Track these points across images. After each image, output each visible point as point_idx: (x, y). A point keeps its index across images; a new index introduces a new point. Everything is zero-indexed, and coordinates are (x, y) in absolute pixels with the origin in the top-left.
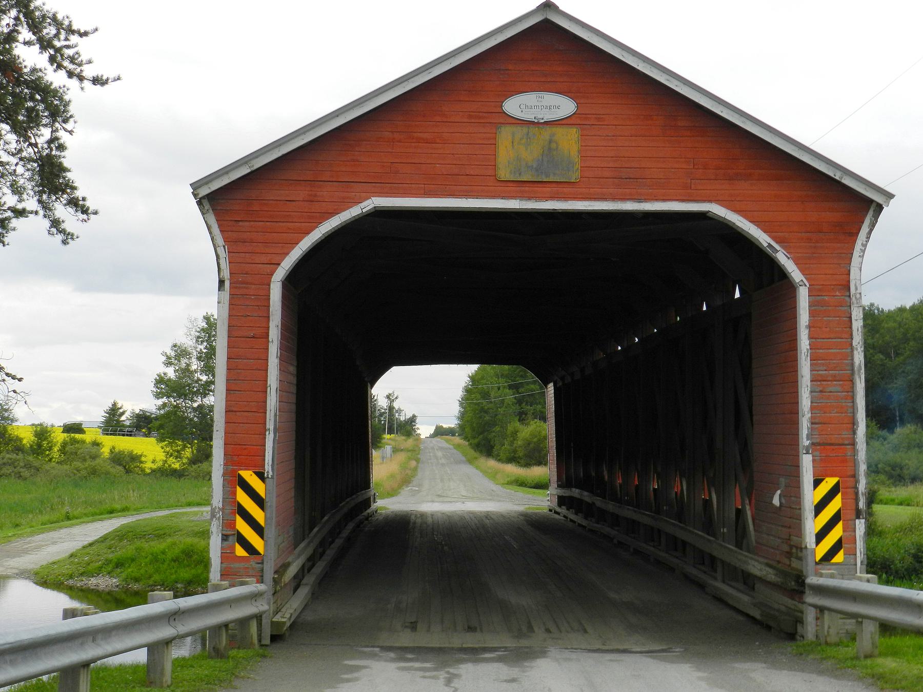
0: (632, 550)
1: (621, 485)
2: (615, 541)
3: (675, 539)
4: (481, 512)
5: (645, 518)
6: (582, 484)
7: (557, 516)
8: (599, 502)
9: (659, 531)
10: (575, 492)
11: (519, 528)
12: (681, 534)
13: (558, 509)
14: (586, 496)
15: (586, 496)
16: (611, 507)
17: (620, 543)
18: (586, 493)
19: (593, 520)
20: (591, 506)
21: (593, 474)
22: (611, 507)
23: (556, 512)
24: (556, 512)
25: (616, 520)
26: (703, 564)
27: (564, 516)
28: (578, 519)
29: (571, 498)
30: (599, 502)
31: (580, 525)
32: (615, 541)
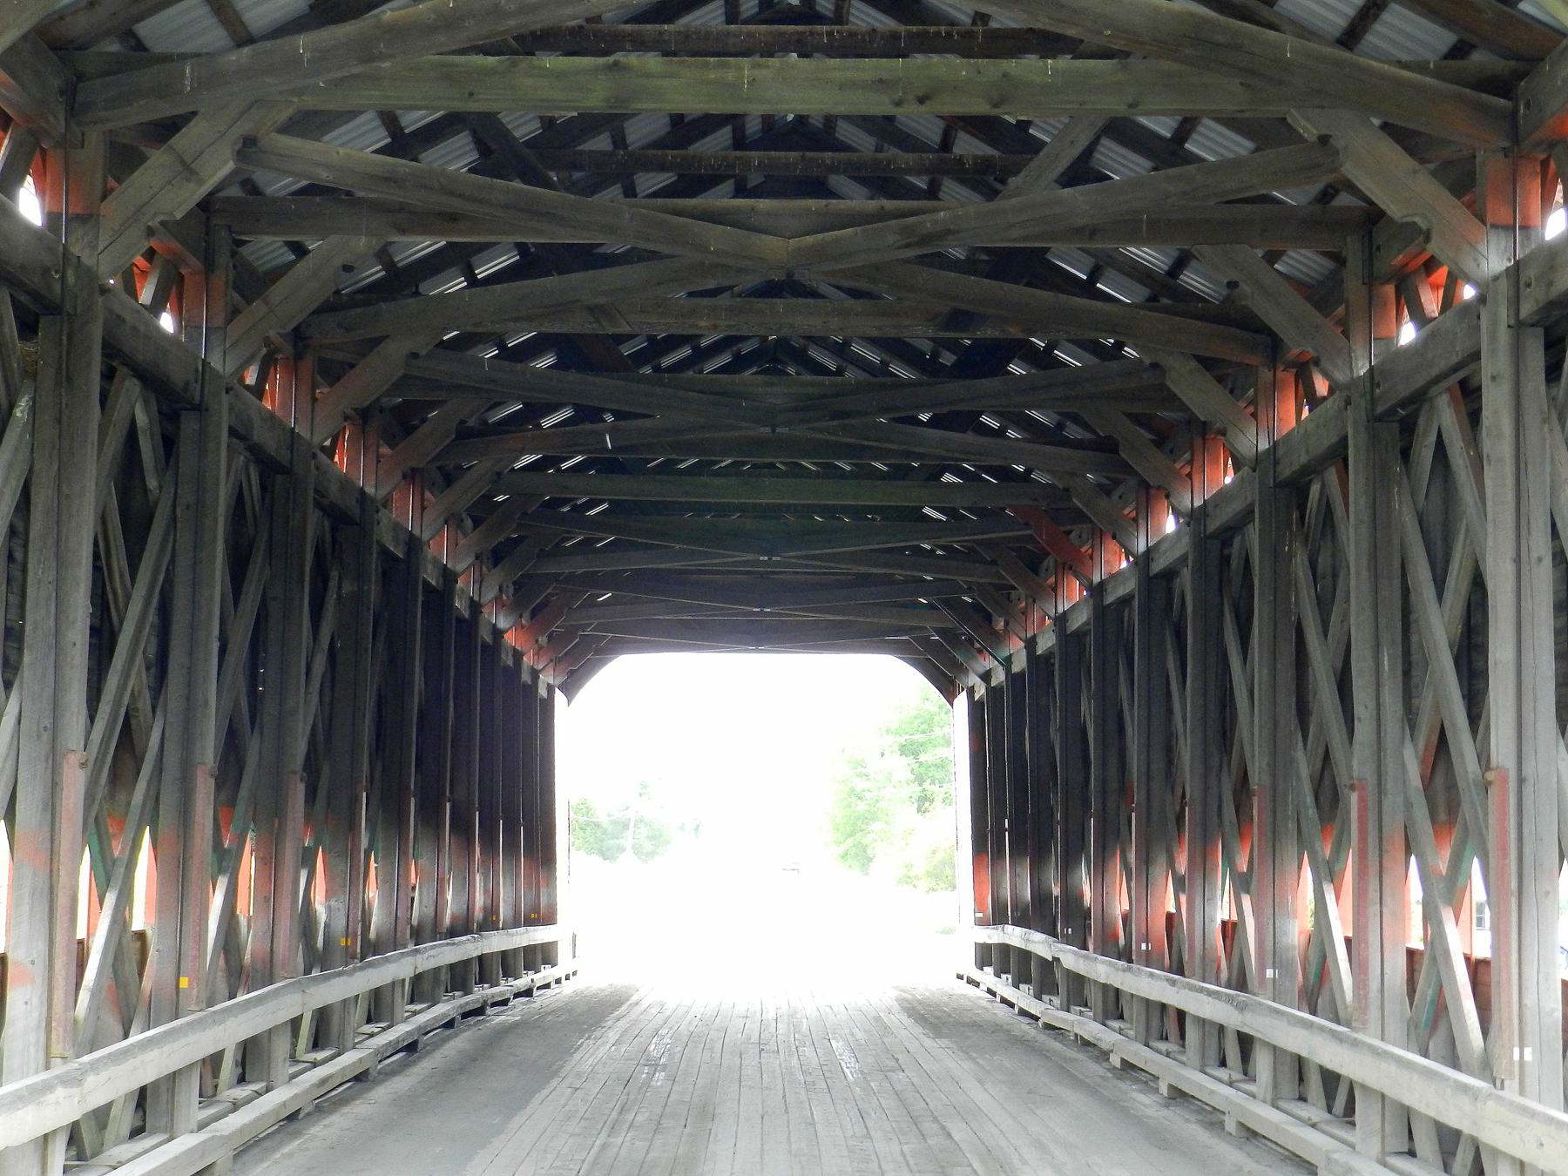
0: (1164, 1090)
1: (1126, 919)
2: (1115, 1060)
3: (1300, 1063)
4: (610, 660)
5: (1202, 1002)
6: (1037, 914)
7: (971, 990)
8: (1070, 958)
9: (1181, 1015)
10: (1014, 936)
11: (878, 1019)
12: (1326, 1053)
13: (976, 974)
14: (1039, 943)
15: (1039, 943)
16: (1101, 969)
17: (1127, 1066)
18: (1038, 937)
19: (1057, 1001)
20: (1049, 966)
21: (1056, 891)
22: (1101, 969)
23: (970, 981)
24: (970, 981)
25: (1114, 1005)
26: (1223, 1064)
27: (990, 991)
28: (1023, 997)
29: (1005, 949)
30: (1070, 958)
31: (1023, 1013)
32: (1115, 1060)
